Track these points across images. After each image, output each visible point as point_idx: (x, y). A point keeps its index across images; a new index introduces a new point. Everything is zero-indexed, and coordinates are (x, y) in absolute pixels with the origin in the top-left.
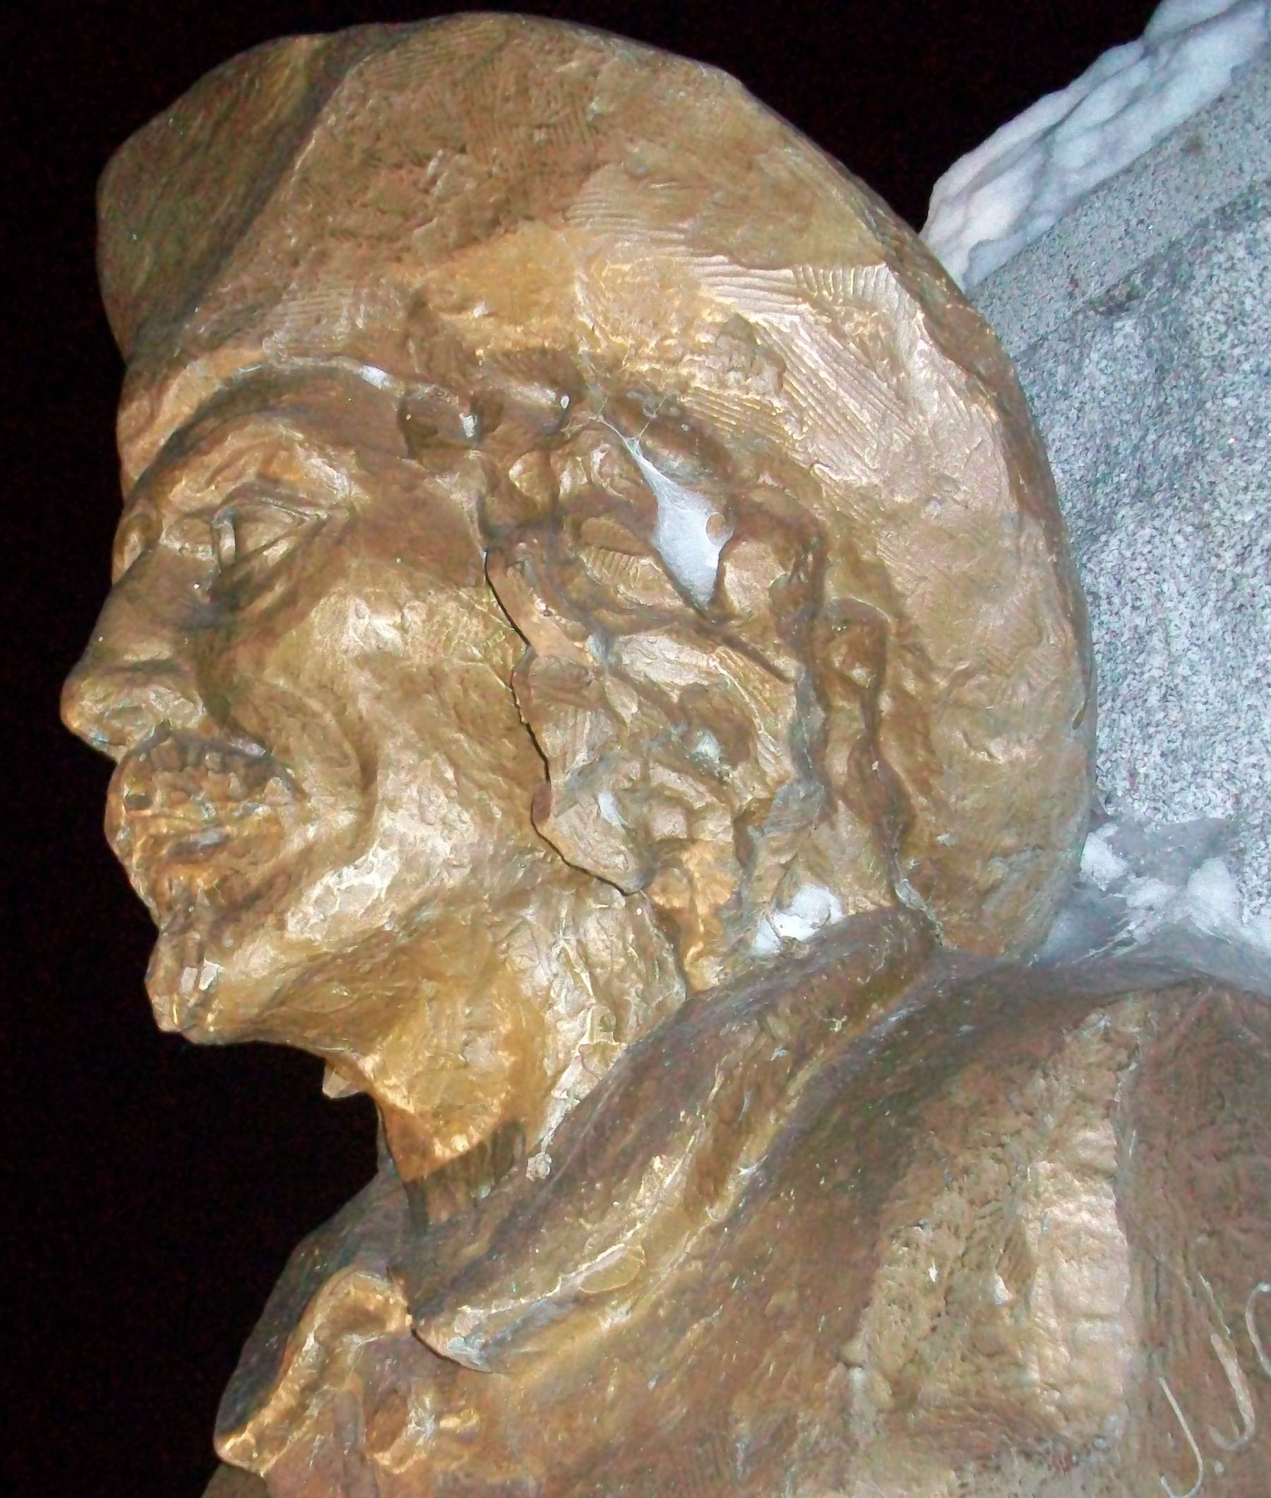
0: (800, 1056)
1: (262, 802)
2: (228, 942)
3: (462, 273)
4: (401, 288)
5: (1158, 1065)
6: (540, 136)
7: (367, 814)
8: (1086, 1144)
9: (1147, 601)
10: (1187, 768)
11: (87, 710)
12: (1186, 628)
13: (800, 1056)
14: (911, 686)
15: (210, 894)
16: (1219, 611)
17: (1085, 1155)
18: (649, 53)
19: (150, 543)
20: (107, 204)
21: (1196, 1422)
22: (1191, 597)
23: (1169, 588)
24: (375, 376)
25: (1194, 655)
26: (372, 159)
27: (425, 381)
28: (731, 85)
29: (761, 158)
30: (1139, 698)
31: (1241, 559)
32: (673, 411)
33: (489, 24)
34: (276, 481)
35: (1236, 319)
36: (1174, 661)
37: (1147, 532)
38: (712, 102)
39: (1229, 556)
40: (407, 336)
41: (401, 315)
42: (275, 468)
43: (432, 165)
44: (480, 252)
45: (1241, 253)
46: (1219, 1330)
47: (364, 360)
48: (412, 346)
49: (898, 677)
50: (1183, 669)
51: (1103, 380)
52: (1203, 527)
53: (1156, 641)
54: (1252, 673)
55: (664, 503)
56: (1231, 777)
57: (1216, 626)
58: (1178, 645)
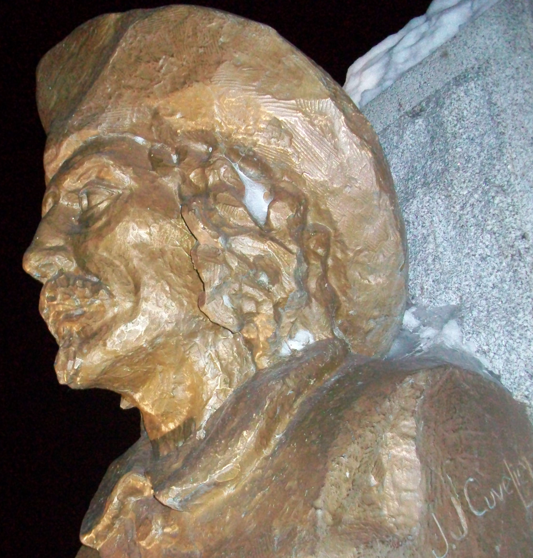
0: (298, 393)
1: (98, 299)
2: (85, 351)
3: (172, 102)
4: (149, 107)
5: (431, 397)
6: (201, 51)
7: (137, 303)
8: (405, 426)
9: (427, 224)
10: (442, 286)
11: (32, 264)
12: (442, 234)
13: (298, 393)
14: (339, 255)
15: (78, 333)
16: (454, 228)
17: (404, 430)
18: (242, 20)
19: (56, 202)
20: (40, 76)
21: (446, 530)
22: (444, 222)
23: (436, 219)
24: (140, 140)
25: (445, 244)
26: (138, 59)
27: (159, 142)
28: (272, 31)
29: (283, 59)
30: (425, 260)
31: (462, 208)
32: (251, 153)
33: (182, 9)
34: (103, 179)
35: (460, 119)
36: (437, 246)
37: (427, 198)
38: (265, 38)
39: (458, 207)
40: (152, 125)
41: (149, 117)
42: (102, 174)
43: (161, 61)
44: (179, 94)
45: (462, 94)
46: (454, 495)
47: (136, 134)
48: (153, 129)
49: (335, 252)
50: (441, 249)
51: (411, 142)
52: (448, 196)
53: (431, 239)
54: (466, 251)
55: (248, 187)
56: (459, 290)
57: (453, 233)
58: (439, 240)
